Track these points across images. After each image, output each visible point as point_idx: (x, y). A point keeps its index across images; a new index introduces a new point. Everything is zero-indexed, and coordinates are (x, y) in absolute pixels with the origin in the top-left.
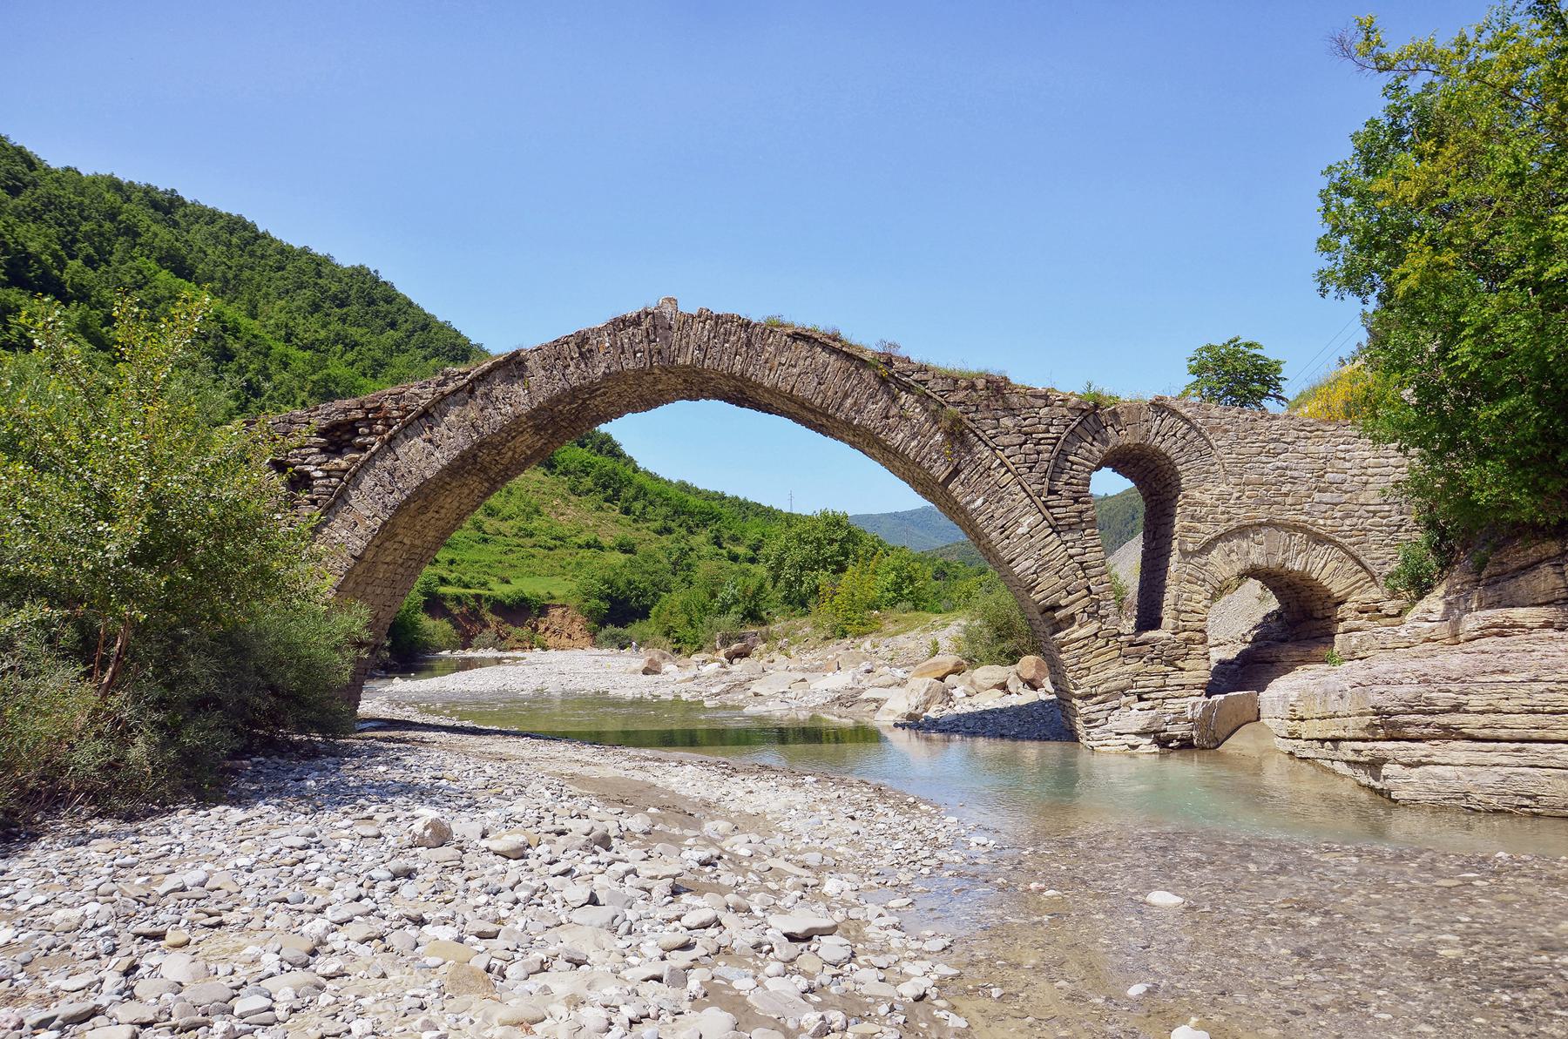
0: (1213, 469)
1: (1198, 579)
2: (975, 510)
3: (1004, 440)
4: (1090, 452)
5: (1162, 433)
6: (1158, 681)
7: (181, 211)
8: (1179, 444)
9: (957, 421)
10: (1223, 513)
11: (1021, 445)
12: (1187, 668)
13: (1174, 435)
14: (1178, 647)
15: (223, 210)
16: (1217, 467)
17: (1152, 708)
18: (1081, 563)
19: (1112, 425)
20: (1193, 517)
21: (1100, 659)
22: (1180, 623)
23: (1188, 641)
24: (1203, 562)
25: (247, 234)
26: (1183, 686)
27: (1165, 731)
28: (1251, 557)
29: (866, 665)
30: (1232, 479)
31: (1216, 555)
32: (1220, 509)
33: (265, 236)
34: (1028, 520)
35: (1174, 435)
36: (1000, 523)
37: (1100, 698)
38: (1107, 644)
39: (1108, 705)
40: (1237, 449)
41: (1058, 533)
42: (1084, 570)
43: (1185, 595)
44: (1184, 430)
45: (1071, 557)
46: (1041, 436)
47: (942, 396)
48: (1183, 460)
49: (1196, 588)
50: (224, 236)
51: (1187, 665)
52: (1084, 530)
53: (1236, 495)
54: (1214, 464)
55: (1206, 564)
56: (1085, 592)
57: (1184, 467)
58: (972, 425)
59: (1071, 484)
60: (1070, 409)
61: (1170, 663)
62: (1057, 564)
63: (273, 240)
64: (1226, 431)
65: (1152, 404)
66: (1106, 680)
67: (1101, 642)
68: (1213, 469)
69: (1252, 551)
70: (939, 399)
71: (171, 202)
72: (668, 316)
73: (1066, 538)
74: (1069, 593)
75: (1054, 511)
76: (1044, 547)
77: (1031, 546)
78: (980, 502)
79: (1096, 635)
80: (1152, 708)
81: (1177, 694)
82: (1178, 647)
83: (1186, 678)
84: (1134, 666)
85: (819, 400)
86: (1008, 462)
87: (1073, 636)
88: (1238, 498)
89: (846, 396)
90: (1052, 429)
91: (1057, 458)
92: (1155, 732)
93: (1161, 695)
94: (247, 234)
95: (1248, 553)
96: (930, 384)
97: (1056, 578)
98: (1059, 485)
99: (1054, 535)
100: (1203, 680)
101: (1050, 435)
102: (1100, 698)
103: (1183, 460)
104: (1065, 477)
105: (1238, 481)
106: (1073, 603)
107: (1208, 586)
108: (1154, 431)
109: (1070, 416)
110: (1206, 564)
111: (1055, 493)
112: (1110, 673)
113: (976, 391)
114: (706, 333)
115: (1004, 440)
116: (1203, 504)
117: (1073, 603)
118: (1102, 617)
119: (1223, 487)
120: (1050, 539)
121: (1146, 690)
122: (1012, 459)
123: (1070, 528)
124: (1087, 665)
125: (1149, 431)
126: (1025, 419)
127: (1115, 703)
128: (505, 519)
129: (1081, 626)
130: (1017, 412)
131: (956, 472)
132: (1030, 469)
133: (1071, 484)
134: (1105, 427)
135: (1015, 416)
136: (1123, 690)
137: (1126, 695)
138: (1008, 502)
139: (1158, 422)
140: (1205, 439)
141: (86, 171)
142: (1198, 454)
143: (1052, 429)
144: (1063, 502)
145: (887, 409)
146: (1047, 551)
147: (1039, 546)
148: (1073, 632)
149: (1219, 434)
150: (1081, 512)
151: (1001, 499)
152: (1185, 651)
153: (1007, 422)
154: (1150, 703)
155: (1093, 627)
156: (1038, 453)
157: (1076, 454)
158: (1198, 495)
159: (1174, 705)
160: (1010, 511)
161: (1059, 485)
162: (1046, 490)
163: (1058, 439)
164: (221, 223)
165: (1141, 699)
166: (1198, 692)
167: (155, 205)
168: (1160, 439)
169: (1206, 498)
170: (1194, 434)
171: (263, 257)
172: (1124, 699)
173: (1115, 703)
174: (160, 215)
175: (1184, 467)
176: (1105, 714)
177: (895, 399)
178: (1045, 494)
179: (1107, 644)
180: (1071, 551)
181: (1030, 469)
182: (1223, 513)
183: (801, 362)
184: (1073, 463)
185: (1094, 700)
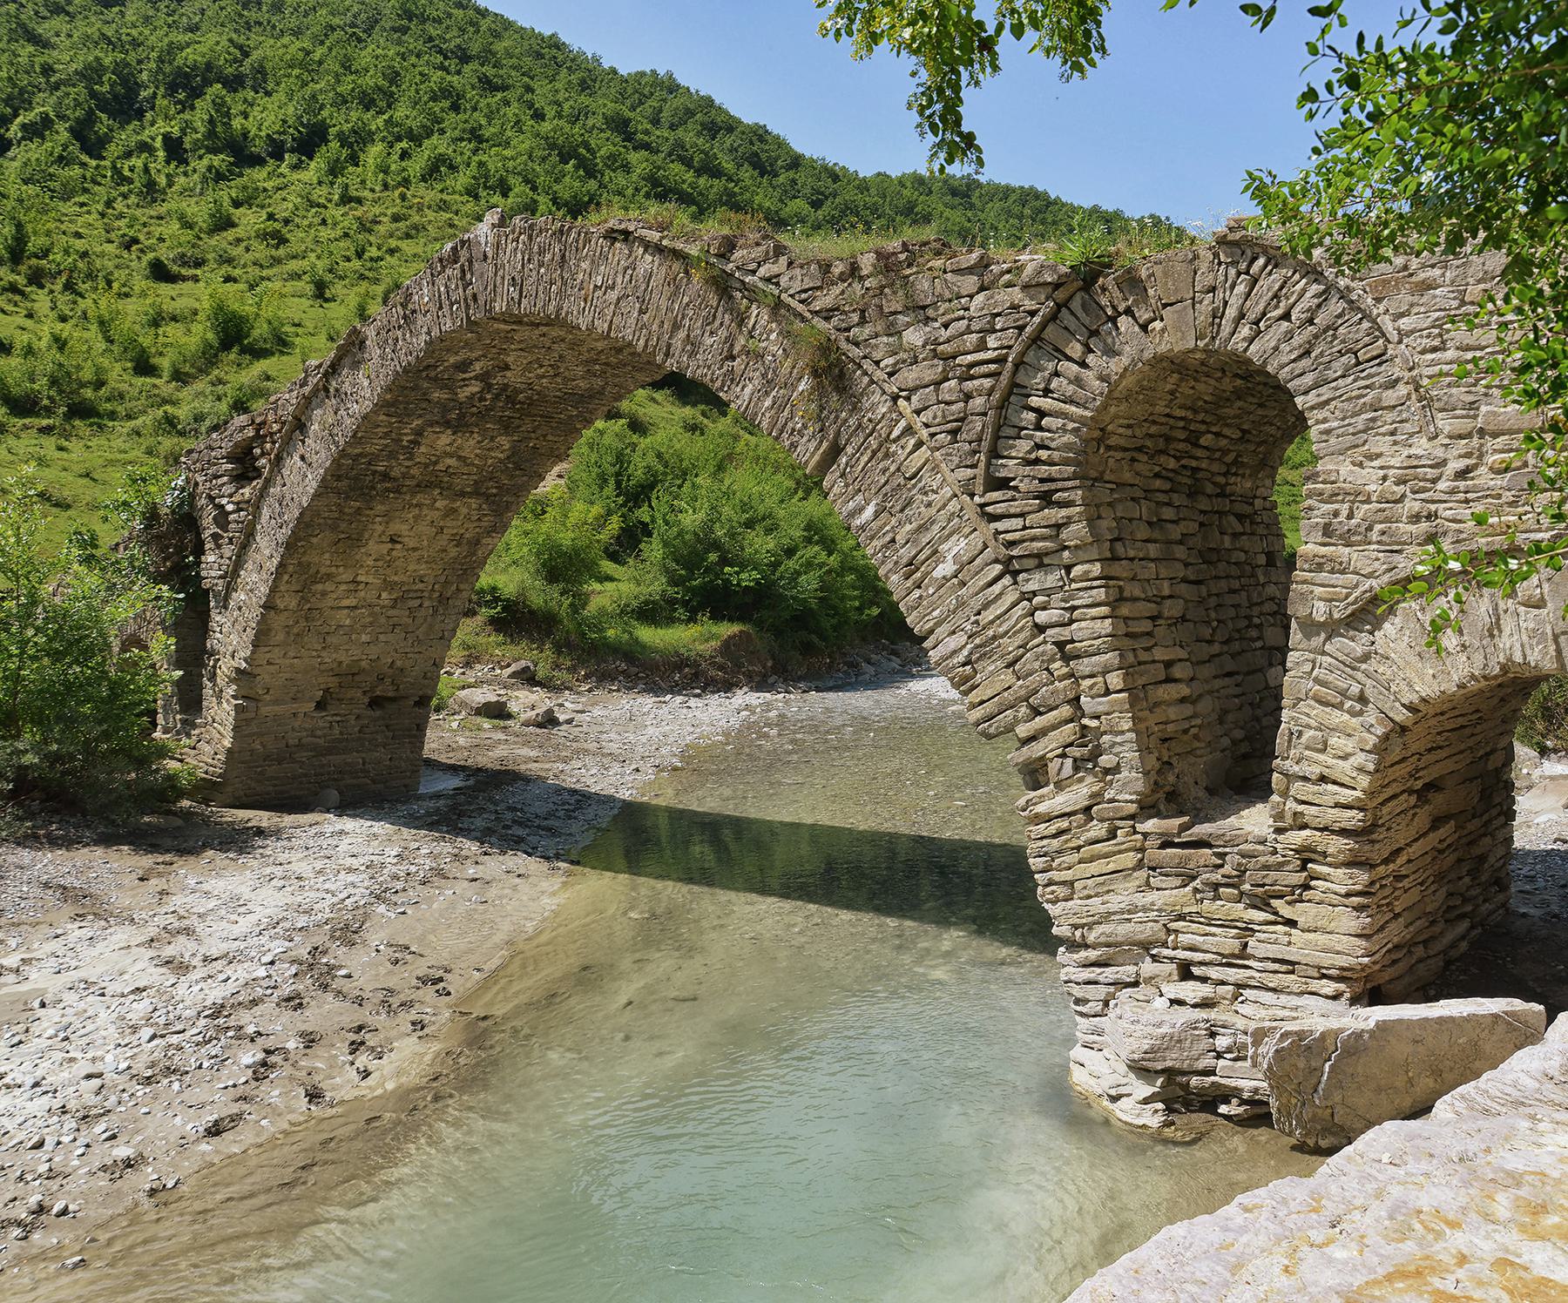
0: (1390, 397)
1: (1344, 693)
2: (863, 528)
3: (909, 376)
4: (1078, 381)
5: (1252, 316)
6: (1226, 941)
7: (977, 194)
8: (1296, 341)
9: (827, 348)
10: (1415, 518)
11: (938, 384)
12: (1301, 920)
13: (1286, 316)
14: (1279, 867)
15: (1015, 183)
16: (1402, 390)
17: (1206, 1004)
18: (1060, 645)
19: (1129, 312)
20: (1327, 530)
21: (1094, 868)
22: (1291, 805)
23: (1306, 856)
24: (1359, 650)
25: (1038, 203)
26: (1291, 966)
27: (1211, 1072)
28: (1505, 642)
29: (319, 865)
30: (1445, 423)
31: (1395, 635)
32: (1412, 505)
33: (1057, 202)
34: (956, 547)
35: (1286, 316)
36: (906, 553)
37: (1093, 954)
38: (1112, 835)
39: (1109, 973)
40: (1460, 334)
41: (1015, 574)
42: (1067, 658)
43: (1308, 734)
44: (1308, 301)
45: (1040, 629)
46: (970, 358)
47: (802, 302)
48: (1308, 379)
49: (1338, 717)
50: (1016, 209)
51: (1303, 913)
52: (1068, 568)
53: (1455, 465)
54: (1393, 384)
55: (1366, 658)
56: (1066, 711)
57: (1312, 399)
58: (856, 352)
59: (1037, 461)
60: (1025, 287)
61: (1262, 903)
62: (1010, 645)
63: (1064, 205)
64: (1427, 286)
65: (1222, 241)
66: (1106, 917)
67: (1097, 829)
68: (1390, 397)
69: (1508, 624)
70: (800, 308)
71: (968, 186)
72: (483, 241)
73: (1032, 586)
74: (1037, 712)
75: (1000, 526)
76: (986, 606)
77: (961, 604)
78: (869, 511)
79: (1088, 809)
80: (1206, 1004)
81: (1273, 981)
82: (1279, 867)
83: (1300, 946)
84: (1169, 895)
85: (642, 342)
86: (918, 422)
87: (1040, 808)
88: (1462, 474)
89: (676, 326)
90: (992, 342)
91: (1002, 405)
92: (1169, 1072)
93: (1233, 974)
94: (1038, 203)
95: (1494, 630)
96: (784, 281)
97: (1007, 677)
98: (1009, 467)
99: (1007, 580)
100: (1343, 961)
101: (990, 355)
102: (1093, 954)
103: (1308, 379)
104: (1023, 446)
105: (1464, 425)
106: (1043, 732)
107: (1371, 717)
108: (1231, 312)
109: (1029, 305)
110: (1366, 658)
111: (1003, 484)
112: (1116, 902)
113: (861, 279)
114: (519, 256)
115: (909, 376)
116: (1358, 496)
117: (1043, 732)
118: (1107, 771)
119: (1421, 446)
120: (997, 588)
121: (1198, 956)
122: (924, 417)
123: (1040, 561)
124: (1066, 875)
125: (1217, 315)
126: (946, 326)
127: (1126, 972)
128: (1295, 467)
129: (1060, 786)
130: (930, 312)
131: (835, 451)
132: (954, 433)
133: (1037, 461)
134: (1113, 319)
135: (927, 320)
136: (1146, 946)
137: (1155, 958)
138: (919, 510)
139: (1241, 289)
140: (1366, 316)
141: (895, 173)
142: (1348, 359)
143: (992, 342)
144: (1015, 507)
145: (730, 340)
146: (988, 615)
147: (976, 603)
148: (1042, 799)
149: (1403, 299)
150: (1058, 527)
151: (909, 503)
152: (1299, 878)
153: (914, 337)
154: (1205, 990)
155: (1077, 795)
156: (968, 397)
157: (1047, 392)
158: (1346, 469)
159: (1255, 1011)
160: (922, 528)
161: (1009, 467)
162: (980, 481)
163: (1001, 360)
164: (1013, 197)
165: (1185, 972)
166: (1329, 987)
167: (954, 192)
168: (1245, 331)
169: (1369, 479)
170: (1336, 306)
171: (1054, 223)
172: (1148, 967)
173: (1126, 972)
174: (957, 200)
175: (1312, 399)
176: (1101, 991)
177: (741, 320)
178: (979, 489)
179: (1112, 835)
180: (1041, 617)
181: (954, 433)
182: (1415, 518)
183: (619, 280)
184: (1041, 414)
185: (1083, 954)
